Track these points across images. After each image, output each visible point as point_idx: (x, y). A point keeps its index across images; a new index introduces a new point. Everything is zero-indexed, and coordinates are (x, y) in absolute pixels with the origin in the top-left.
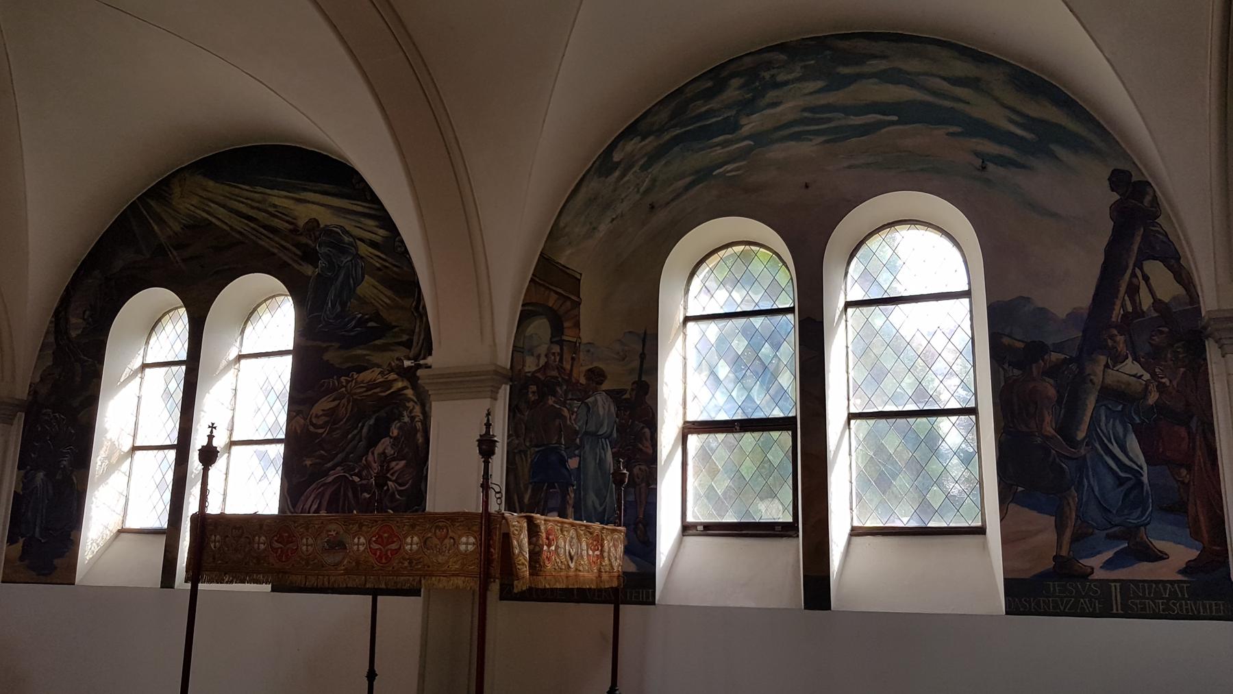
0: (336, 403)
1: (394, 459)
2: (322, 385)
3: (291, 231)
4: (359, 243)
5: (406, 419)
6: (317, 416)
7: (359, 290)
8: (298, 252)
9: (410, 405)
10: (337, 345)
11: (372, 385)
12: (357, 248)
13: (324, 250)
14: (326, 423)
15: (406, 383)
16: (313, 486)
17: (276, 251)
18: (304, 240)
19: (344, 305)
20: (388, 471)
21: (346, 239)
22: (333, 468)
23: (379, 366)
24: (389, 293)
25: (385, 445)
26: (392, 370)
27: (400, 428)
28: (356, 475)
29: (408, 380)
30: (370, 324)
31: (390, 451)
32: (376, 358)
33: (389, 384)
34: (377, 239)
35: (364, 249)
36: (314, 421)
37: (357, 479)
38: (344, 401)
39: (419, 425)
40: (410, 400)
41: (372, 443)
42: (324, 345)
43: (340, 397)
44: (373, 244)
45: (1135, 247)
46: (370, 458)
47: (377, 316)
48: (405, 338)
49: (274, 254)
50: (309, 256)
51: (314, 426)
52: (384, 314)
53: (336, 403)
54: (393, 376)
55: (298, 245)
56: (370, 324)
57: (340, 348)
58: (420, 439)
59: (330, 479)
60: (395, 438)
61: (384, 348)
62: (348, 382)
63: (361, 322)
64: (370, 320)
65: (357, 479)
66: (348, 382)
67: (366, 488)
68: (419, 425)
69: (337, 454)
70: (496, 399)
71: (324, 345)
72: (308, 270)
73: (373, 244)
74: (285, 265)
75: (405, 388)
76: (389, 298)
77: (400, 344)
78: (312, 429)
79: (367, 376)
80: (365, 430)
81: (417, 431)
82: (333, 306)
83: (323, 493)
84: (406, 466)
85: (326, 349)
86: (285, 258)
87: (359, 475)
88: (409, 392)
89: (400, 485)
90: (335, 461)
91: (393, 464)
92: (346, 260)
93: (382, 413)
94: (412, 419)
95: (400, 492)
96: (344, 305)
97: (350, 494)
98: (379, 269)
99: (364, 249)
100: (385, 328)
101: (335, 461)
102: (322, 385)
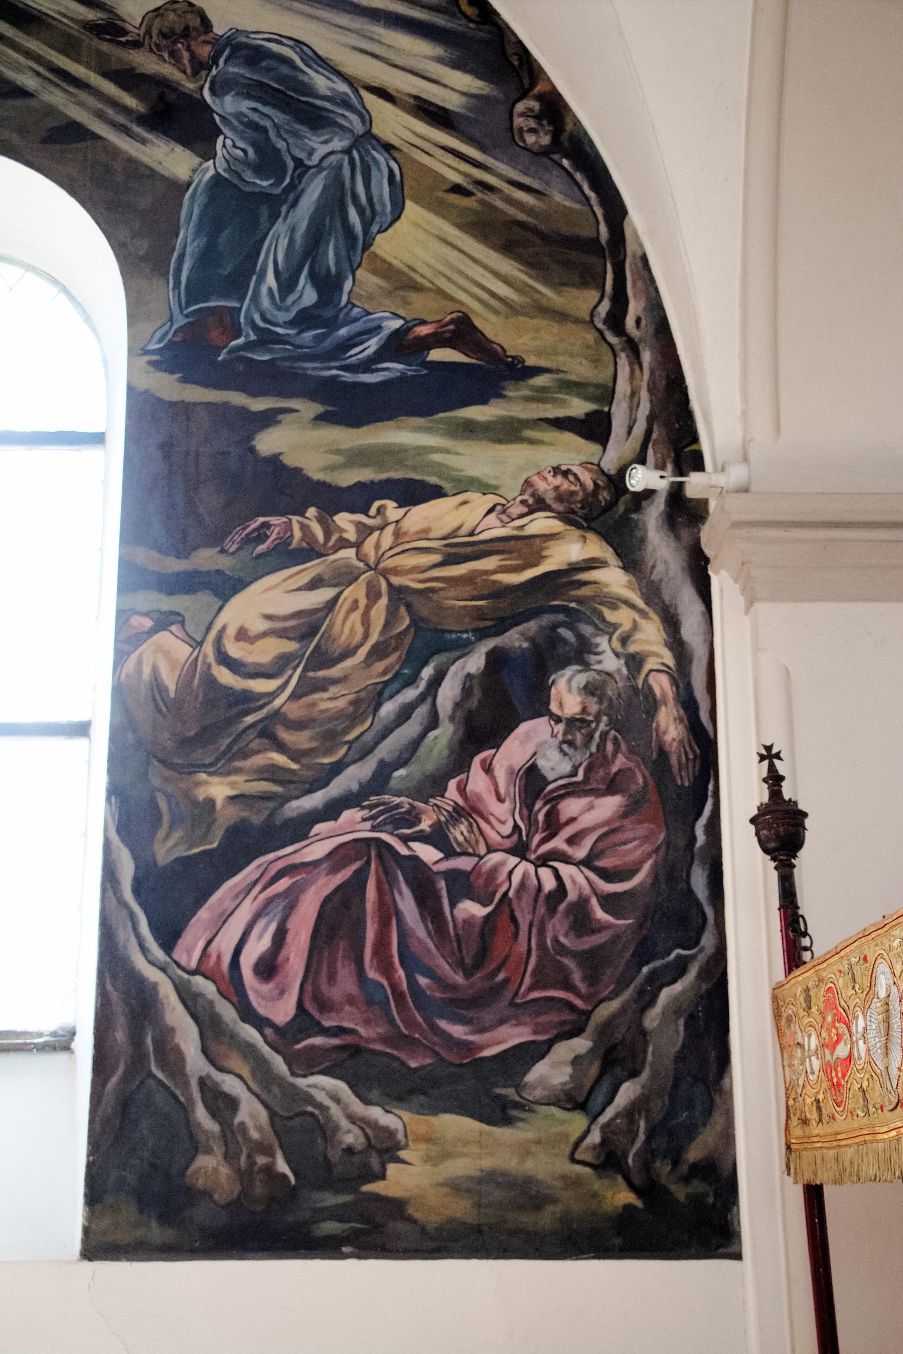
0: (324, 595)
1: (572, 790)
2: (261, 535)
3: (92, 28)
4: (370, 99)
5: (610, 662)
6: (242, 635)
7: (387, 245)
8: (130, 101)
9: (623, 617)
10: (314, 408)
11: (459, 549)
12: (366, 117)
13: (229, 105)
14: (282, 663)
15: (595, 548)
16: (250, 871)
17: (30, 82)
18: (149, 63)
19: (327, 286)
20: (553, 826)
21: (321, 82)
22: (331, 811)
23: (485, 488)
24: (508, 266)
25: (531, 742)
26: (539, 505)
27: (589, 690)
28: (421, 837)
29: (606, 536)
30: (438, 355)
31: (555, 766)
32: (474, 459)
33: (528, 548)
34: (452, 102)
35: (392, 123)
36: (234, 650)
37: (428, 853)
38: (357, 591)
39: (661, 685)
40: (615, 603)
41: (484, 728)
42: (259, 405)
43: (344, 577)
44: (425, 110)
45: (411, 1004)
46: (477, 781)
47: (462, 332)
48: (579, 407)
49: (23, 93)
50: (177, 117)
51: (225, 660)
52: (491, 326)
53: (324, 595)
54: (541, 523)
55: (128, 79)
56: (438, 355)
57: (322, 419)
58: (670, 726)
59: (316, 850)
60: (572, 723)
61: (509, 432)
62: (365, 531)
63: (400, 345)
64: (437, 340)
65: (428, 853)
66: (365, 531)
67: (462, 885)
68: (661, 685)
69: (337, 768)
70: (84, 28)
71: (259, 405)
72: (173, 160)
73: (425, 110)
74: (74, 132)
75: (592, 564)
76: (506, 280)
77: (560, 424)
78: (225, 676)
79: (437, 516)
80: (449, 692)
81: (652, 705)
82: (287, 284)
83: (291, 899)
84: (625, 813)
85: (268, 419)
86: (76, 113)
87: (437, 838)
88: (614, 578)
89: (607, 875)
90: (337, 787)
91: (571, 807)
92: (322, 146)
93: (515, 639)
94: (635, 662)
95: (609, 902)
96: (327, 286)
97: (407, 904)
98: (457, 189)
99: (392, 123)
100: (494, 372)
101: (337, 787)
102: (261, 535)
